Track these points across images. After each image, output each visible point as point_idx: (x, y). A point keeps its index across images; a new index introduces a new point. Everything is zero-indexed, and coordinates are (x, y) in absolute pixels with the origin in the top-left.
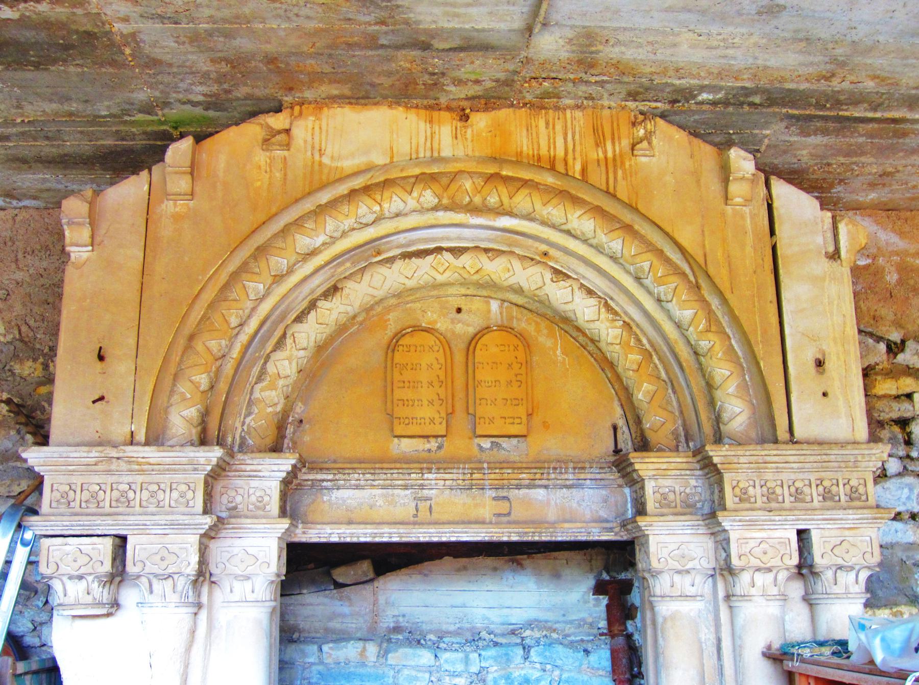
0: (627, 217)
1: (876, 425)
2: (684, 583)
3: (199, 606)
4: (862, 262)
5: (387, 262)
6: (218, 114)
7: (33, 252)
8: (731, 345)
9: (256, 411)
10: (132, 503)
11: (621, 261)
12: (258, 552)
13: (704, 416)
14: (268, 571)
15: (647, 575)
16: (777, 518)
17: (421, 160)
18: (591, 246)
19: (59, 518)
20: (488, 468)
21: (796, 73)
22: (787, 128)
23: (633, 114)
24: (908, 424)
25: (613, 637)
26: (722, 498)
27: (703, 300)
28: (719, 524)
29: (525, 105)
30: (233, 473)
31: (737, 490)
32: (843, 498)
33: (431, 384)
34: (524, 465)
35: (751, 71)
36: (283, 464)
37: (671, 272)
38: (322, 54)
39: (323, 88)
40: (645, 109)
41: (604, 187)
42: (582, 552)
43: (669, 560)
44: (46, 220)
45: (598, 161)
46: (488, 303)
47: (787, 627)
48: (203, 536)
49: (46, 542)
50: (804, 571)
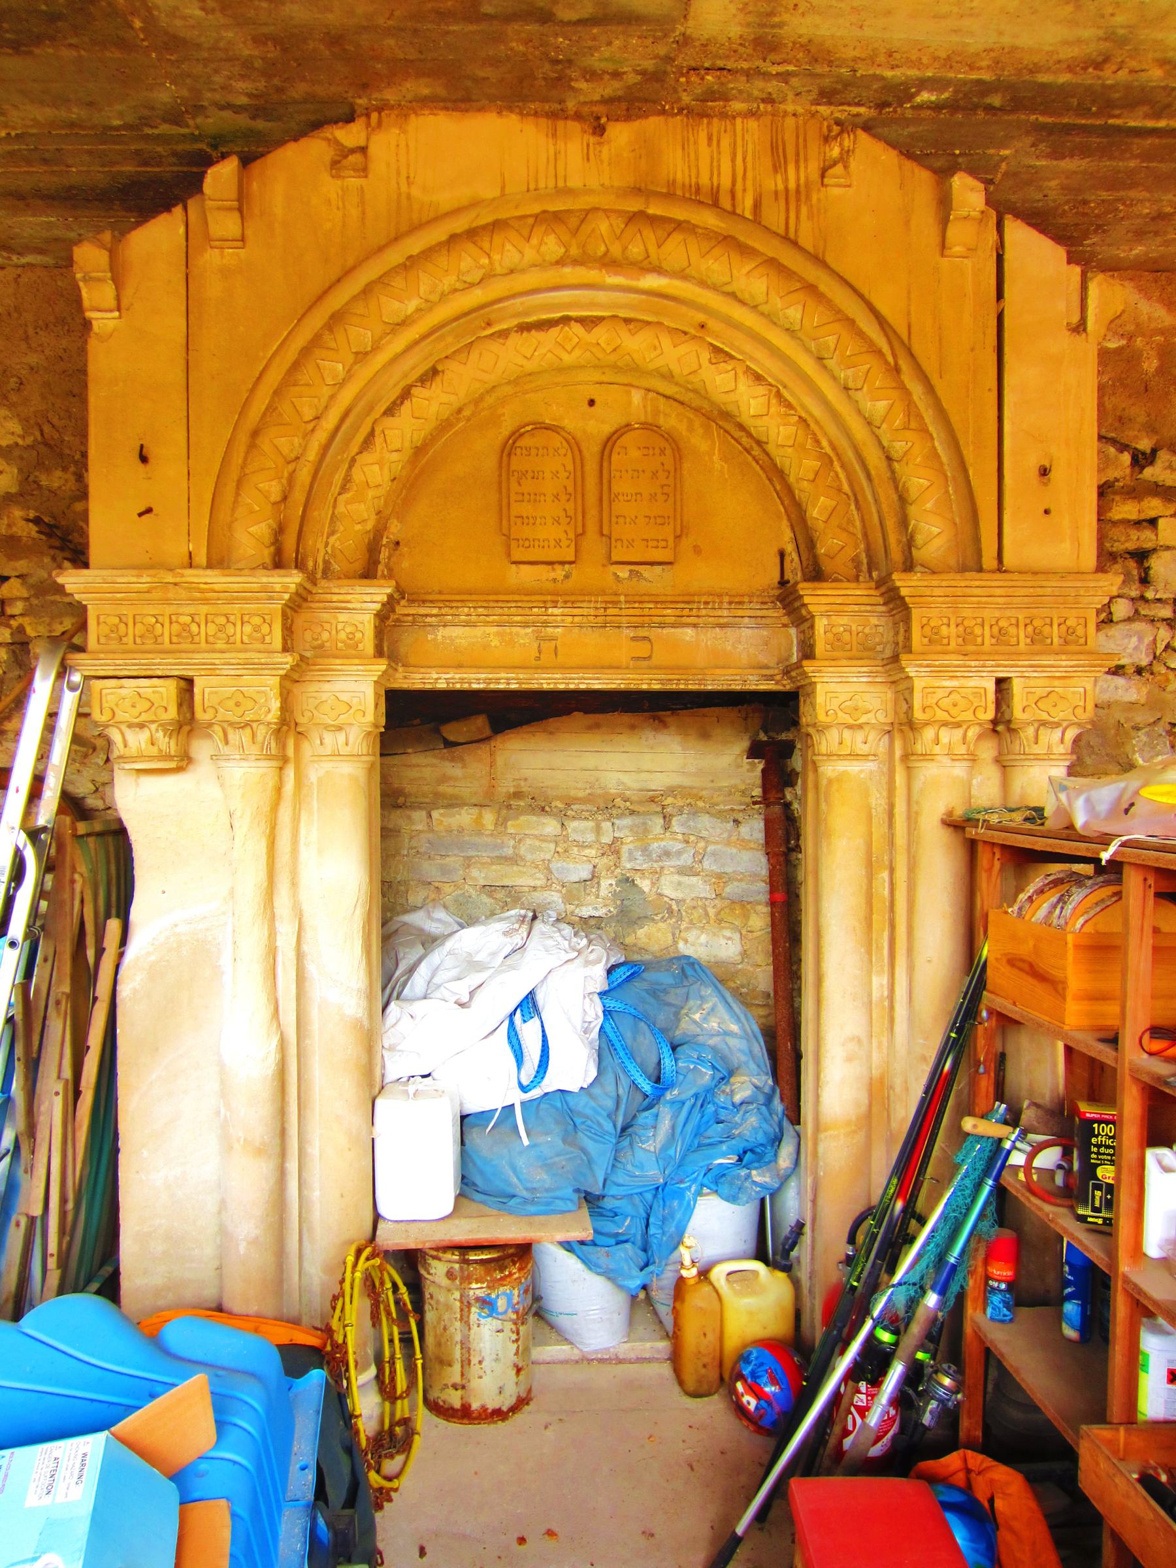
0: (812, 273)
1: (1106, 558)
2: (856, 741)
3: (285, 760)
4: (1112, 345)
5: (499, 337)
6: (269, 125)
7: (47, 325)
8: (934, 448)
9: (342, 529)
10: (197, 639)
11: (799, 334)
12: (352, 696)
13: (892, 539)
14: (363, 720)
15: (811, 730)
16: (973, 663)
17: (542, 192)
18: (762, 314)
19: (111, 656)
20: (626, 602)
21: (1055, 57)
22: (1033, 145)
23: (825, 124)
24: (1147, 557)
25: (768, 806)
26: (908, 638)
27: (902, 387)
28: (902, 669)
29: (681, 110)
30: (317, 605)
31: (927, 629)
32: (1056, 640)
33: (557, 497)
34: (669, 599)
35: (992, 54)
36: (376, 594)
37: (864, 349)
38: (402, 30)
39: (408, 85)
40: (842, 116)
41: (782, 231)
42: (736, 709)
43: (840, 714)
44: (59, 283)
45: (776, 193)
46: (629, 393)
47: (973, 792)
48: (284, 678)
49: (97, 685)
50: (1000, 728)
